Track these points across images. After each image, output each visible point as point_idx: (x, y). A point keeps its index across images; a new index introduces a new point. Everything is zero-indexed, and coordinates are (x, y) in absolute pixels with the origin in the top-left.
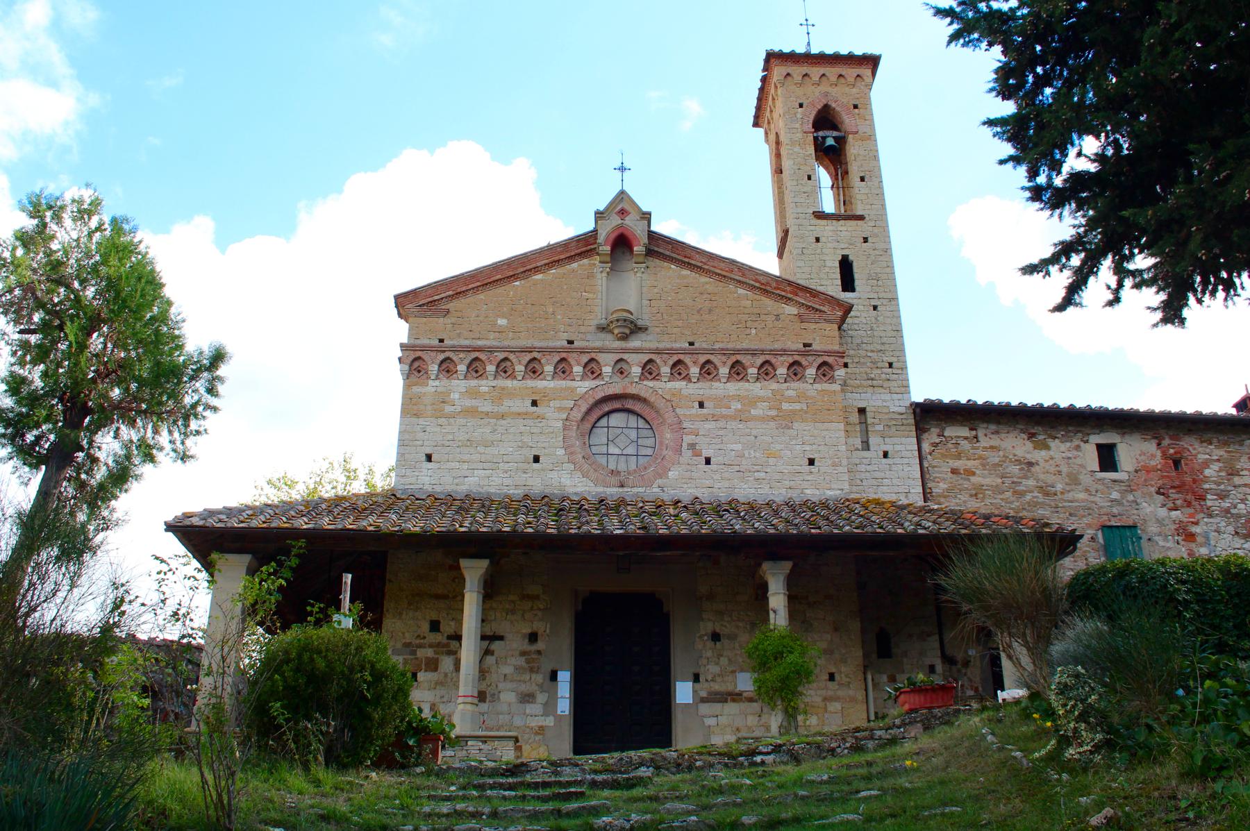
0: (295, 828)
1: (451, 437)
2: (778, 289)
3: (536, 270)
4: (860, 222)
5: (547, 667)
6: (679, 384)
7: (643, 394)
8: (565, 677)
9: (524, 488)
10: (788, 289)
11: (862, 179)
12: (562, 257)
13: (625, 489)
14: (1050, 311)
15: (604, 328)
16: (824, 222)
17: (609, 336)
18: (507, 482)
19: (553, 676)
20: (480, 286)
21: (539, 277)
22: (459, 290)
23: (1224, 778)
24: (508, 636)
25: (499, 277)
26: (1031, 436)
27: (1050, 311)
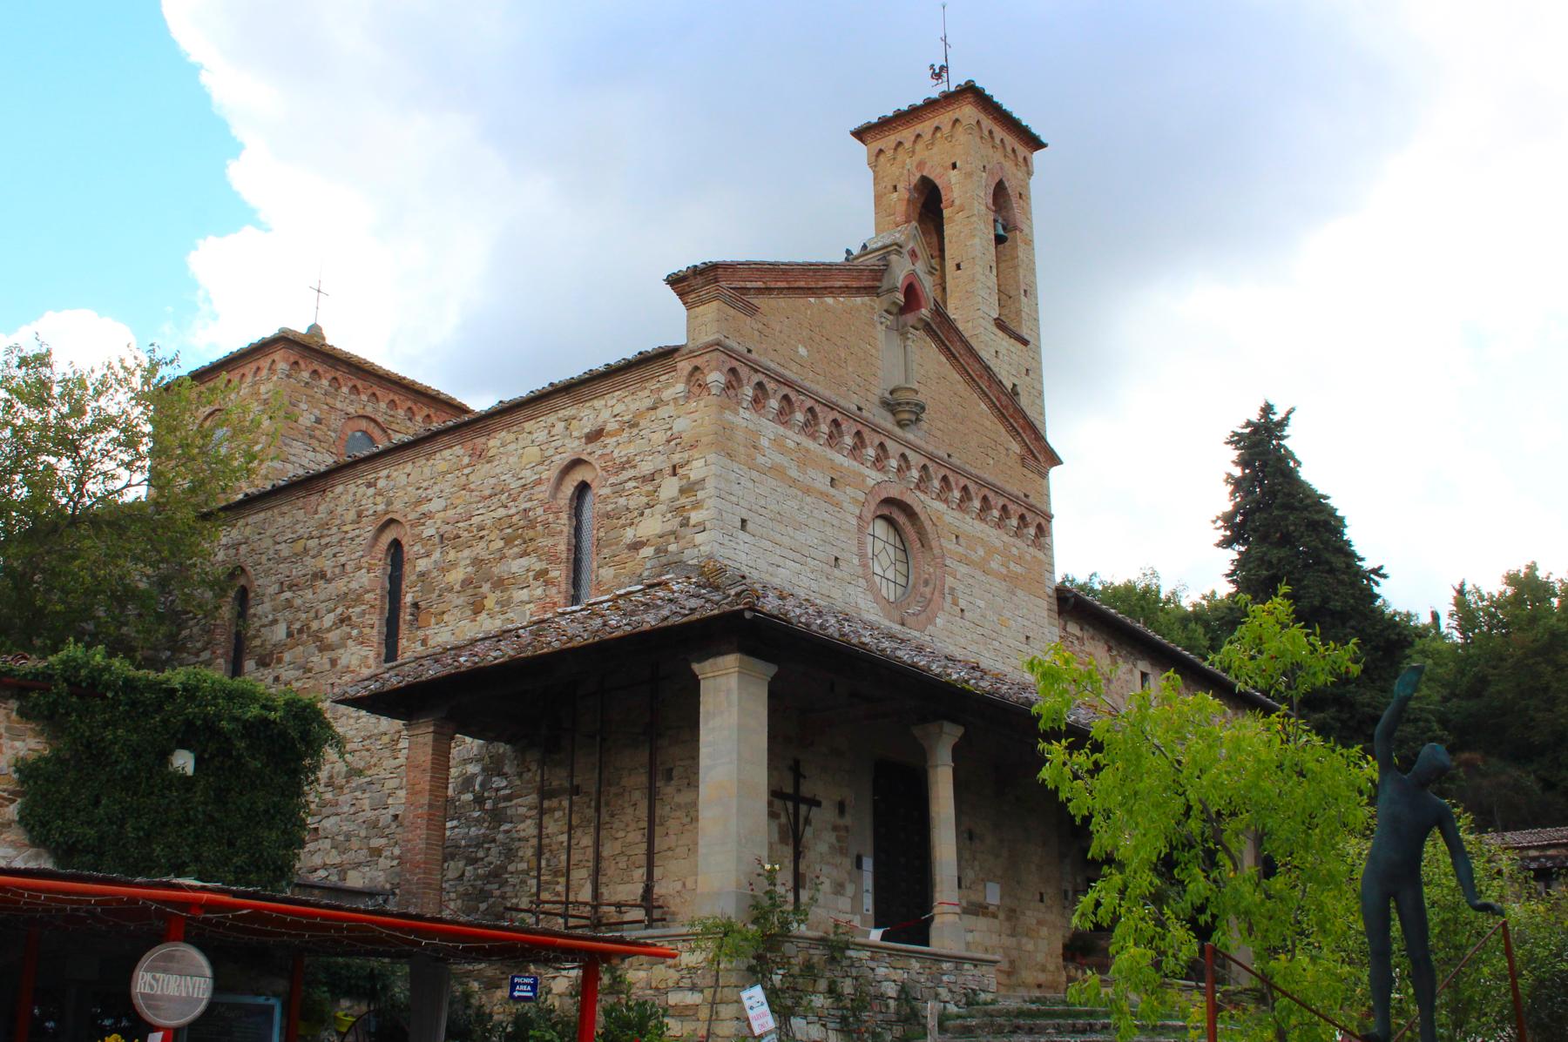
0: (642, 1029)
1: (763, 502)
2: (1013, 417)
3: (830, 291)
4: (1020, 346)
5: (854, 852)
6: (941, 506)
7: (918, 509)
8: (868, 864)
9: (828, 599)
10: (1021, 421)
11: (958, 267)
12: (855, 284)
13: (905, 629)
14: (259, 225)
15: (888, 404)
16: (1000, 334)
17: (889, 416)
18: (814, 586)
19: (859, 865)
20: (784, 288)
21: (830, 300)
22: (772, 285)
23: (820, 993)
24: (825, 803)
25: (802, 284)
26: (1110, 649)
27: (1218, 545)
